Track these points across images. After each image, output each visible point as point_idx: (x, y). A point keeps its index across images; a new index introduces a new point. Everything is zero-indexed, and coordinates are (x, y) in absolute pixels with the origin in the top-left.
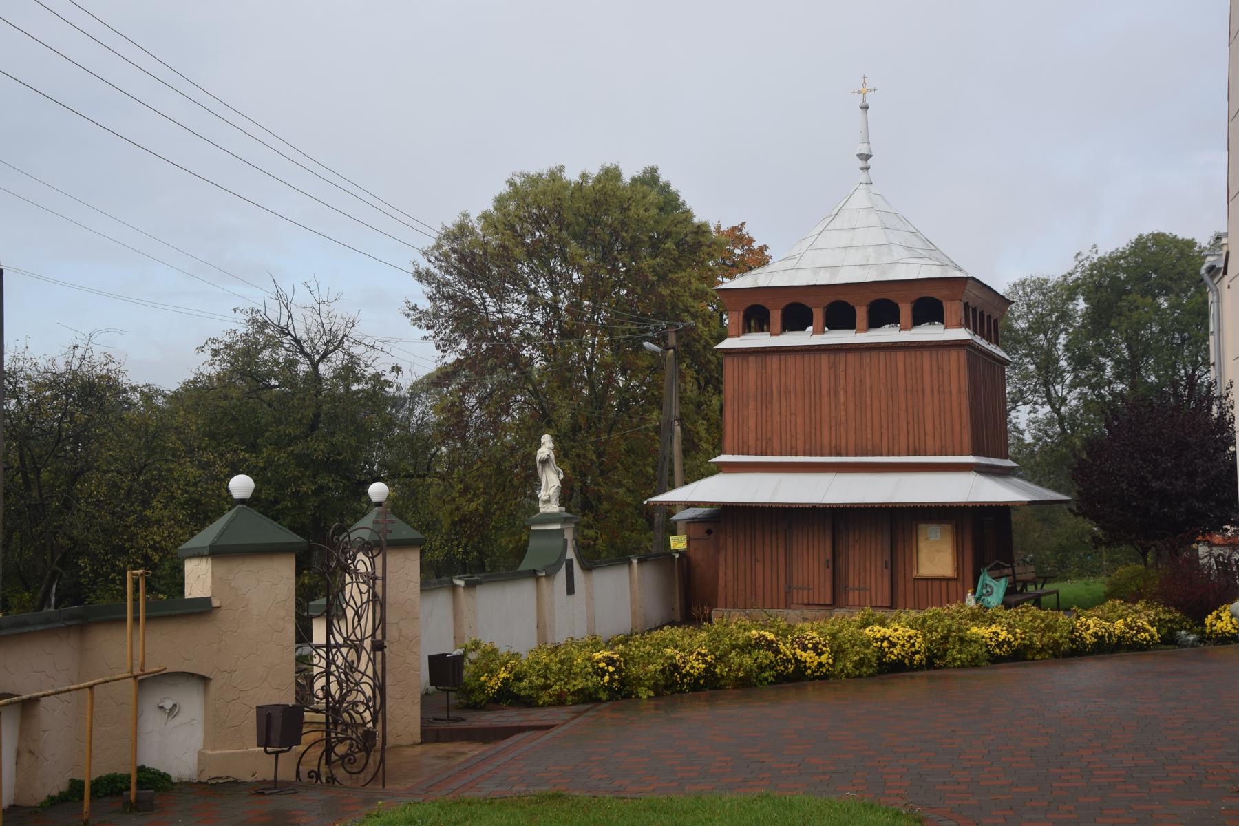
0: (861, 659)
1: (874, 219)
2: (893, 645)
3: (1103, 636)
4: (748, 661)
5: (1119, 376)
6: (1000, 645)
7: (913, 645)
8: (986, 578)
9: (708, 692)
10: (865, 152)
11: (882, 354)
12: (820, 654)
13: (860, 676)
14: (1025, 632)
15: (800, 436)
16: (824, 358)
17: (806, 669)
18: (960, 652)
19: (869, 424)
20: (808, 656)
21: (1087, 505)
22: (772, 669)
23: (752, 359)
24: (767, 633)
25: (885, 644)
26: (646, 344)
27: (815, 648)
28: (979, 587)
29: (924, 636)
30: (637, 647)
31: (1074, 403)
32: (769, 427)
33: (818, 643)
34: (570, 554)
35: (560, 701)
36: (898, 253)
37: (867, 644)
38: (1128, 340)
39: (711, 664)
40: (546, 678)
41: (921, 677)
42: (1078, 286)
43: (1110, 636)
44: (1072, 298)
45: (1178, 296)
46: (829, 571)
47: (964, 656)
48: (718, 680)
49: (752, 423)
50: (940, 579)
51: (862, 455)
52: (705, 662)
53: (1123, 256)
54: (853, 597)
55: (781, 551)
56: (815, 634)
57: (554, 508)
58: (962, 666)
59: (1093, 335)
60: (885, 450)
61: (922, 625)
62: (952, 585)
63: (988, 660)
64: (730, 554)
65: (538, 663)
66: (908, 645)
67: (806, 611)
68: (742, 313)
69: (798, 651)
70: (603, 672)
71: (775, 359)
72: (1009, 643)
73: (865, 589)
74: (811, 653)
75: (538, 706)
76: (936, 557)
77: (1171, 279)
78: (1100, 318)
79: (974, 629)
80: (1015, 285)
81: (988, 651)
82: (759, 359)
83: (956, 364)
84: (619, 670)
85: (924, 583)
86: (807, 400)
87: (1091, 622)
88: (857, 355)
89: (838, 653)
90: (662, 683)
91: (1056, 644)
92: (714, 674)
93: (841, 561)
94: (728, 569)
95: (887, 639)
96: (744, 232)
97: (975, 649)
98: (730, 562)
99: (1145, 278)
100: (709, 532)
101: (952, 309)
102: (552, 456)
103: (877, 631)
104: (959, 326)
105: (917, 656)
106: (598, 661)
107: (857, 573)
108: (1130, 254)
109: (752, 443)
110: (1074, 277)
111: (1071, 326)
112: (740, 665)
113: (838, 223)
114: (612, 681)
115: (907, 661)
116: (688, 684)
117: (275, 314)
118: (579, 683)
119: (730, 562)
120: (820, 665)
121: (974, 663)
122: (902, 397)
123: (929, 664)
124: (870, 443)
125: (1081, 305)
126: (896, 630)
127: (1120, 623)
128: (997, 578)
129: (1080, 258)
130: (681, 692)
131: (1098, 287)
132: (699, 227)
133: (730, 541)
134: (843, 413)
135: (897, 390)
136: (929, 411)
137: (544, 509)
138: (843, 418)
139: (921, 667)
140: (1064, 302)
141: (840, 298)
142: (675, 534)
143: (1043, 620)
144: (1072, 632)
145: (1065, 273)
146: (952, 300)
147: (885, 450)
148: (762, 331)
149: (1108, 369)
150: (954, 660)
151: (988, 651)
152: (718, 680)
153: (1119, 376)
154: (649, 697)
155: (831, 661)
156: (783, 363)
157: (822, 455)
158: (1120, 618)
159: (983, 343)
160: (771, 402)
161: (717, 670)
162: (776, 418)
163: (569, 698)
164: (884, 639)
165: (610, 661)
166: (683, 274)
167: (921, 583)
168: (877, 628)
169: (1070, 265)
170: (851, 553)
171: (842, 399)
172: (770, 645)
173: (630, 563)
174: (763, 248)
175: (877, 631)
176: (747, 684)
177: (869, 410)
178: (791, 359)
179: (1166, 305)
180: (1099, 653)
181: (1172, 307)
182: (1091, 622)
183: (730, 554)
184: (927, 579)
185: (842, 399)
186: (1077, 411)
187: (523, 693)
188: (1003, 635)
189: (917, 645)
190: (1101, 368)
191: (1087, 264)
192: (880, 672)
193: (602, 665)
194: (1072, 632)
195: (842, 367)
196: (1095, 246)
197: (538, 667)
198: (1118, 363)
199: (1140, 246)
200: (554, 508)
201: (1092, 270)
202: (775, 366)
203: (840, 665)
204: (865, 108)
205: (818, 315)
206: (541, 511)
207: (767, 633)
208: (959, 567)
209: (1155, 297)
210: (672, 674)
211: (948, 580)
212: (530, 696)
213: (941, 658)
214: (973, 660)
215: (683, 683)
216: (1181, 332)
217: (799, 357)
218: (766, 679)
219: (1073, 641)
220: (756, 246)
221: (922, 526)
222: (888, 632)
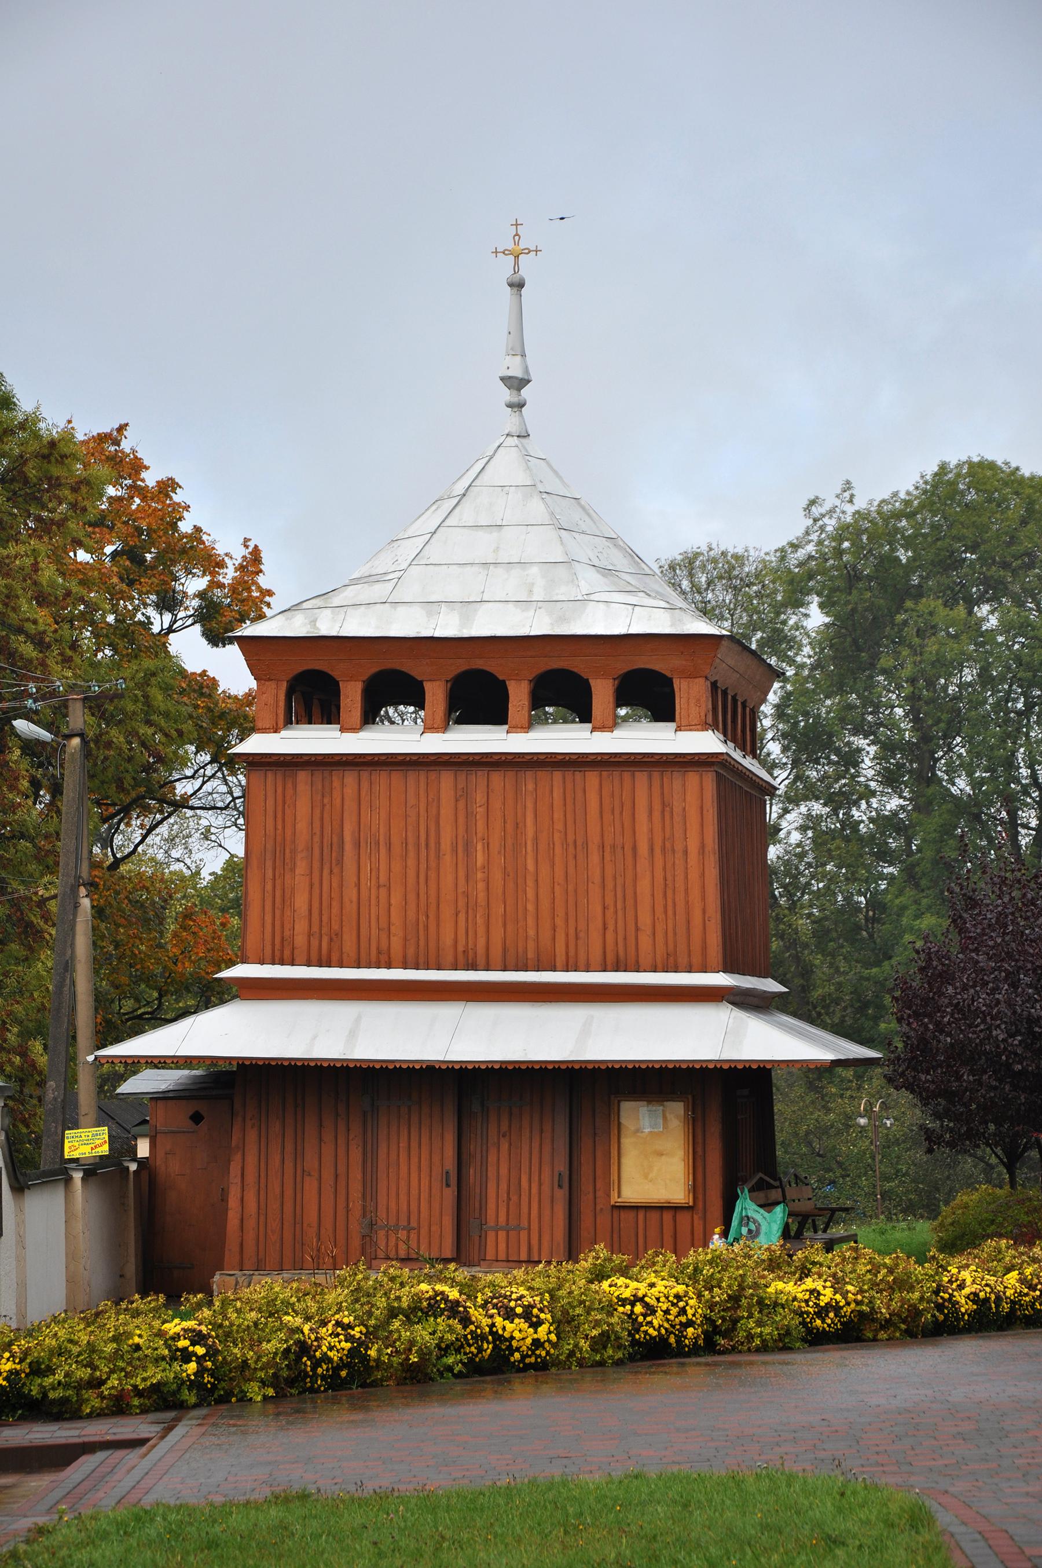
0: (602, 1334)
1: (537, 509)
2: (651, 1310)
3: (987, 1300)
4: (423, 1334)
5: (890, 779)
6: (821, 1312)
7: (683, 1311)
8: (746, 1206)
9: (356, 1391)
10: (517, 372)
11: (558, 775)
12: (536, 1325)
13: (601, 1364)
14: (861, 1291)
15: (397, 930)
16: (446, 779)
17: (512, 1350)
18: (760, 1323)
19: (530, 907)
20: (516, 1329)
21: (915, 1068)
22: (458, 1351)
23: (303, 776)
24: (446, 1289)
25: (639, 1309)
26: (21, 725)
27: (527, 1315)
28: (735, 1223)
29: (699, 1296)
30: (239, 1311)
31: (795, 837)
32: (335, 910)
33: (531, 1306)
35: (118, 1406)
36: (589, 580)
37: (610, 1309)
38: (913, 700)
39: (361, 1343)
40: (95, 1368)
41: (698, 1364)
42: (811, 576)
43: (998, 1299)
44: (796, 602)
45: (1020, 604)
46: (450, 1194)
47: (767, 1330)
48: (369, 1370)
49: (301, 901)
50: (661, 1208)
51: (517, 969)
52: (349, 1338)
53: (907, 511)
54: (496, 1243)
55: (356, 1154)
56: (522, 1291)
58: (764, 1348)
59: (838, 687)
60: (560, 960)
61: (694, 1277)
62: (683, 1218)
63: (804, 1340)
64: (251, 1159)
65: (75, 1343)
66: (674, 1311)
68: (284, 685)
69: (499, 1320)
70: (186, 1356)
71: (350, 778)
72: (837, 1309)
73: (518, 1229)
74: (521, 1323)
75: (81, 1418)
76: (653, 1161)
77: (1005, 565)
78: (853, 650)
79: (780, 1285)
80: (672, 567)
81: (804, 1323)
82: (318, 775)
83: (697, 794)
84: (212, 1353)
85: (632, 1214)
86: (411, 862)
87: (966, 1275)
88: (511, 774)
89: (565, 1323)
90: (285, 1373)
91: (915, 1312)
92: (366, 1358)
93: (472, 1173)
94: (252, 1184)
95: (641, 1300)
96: (126, 445)
97: (785, 1318)
98: (251, 1178)
99: (950, 562)
100: (197, 1118)
101: (690, 694)
103: (624, 1287)
104: (704, 726)
105: (690, 1330)
106: (176, 1337)
107: (503, 1196)
108: (922, 506)
109: (300, 940)
110: (801, 554)
111: (791, 662)
112: (412, 1343)
113: (466, 514)
114: (199, 1373)
115: (672, 1340)
116: (323, 1377)
118: (155, 1375)
119: (251, 1178)
120: (537, 1343)
121: (782, 1344)
122: (595, 858)
123: (708, 1345)
124: (531, 945)
125: (815, 618)
126: (652, 1285)
127: (1013, 1277)
128: (768, 1206)
129: (816, 511)
130: (313, 1390)
131: (853, 577)
132: (53, 444)
133: (252, 1136)
134: (481, 886)
135: (586, 843)
136: (644, 886)
138: (482, 896)
139: (695, 1350)
140: (778, 609)
141: (479, 664)
142: (76, 1126)
143: (891, 1271)
144: (936, 1293)
145: (783, 542)
146: (692, 676)
147: (560, 960)
148: (329, 723)
149: (868, 762)
150: (750, 1337)
151: (804, 1323)
152: (369, 1370)
153: (890, 779)
154: (266, 1398)
155: (553, 1337)
156: (365, 785)
157: (439, 968)
158: (1008, 1270)
159: (737, 755)
160: (340, 862)
161: (373, 1353)
162: (350, 893)
163: (136, 1402)
164: (636, 1299)
165: (198, 1338)
166: (22, 549)
167: (623, 1214)
168: (621, 1281)
169: (796, 526)
170: (492, 1158)
171: (480, 859)
172: (454, 1309)
173: (68, 1180)
174: (168, 486)
175: (624, 1287)
176: (418, 1377)
177: (530, 883)
178: (381, 778)
179: (993, 622)
180: (979, 1330)
181: (1006, 627)
182: (966, 1275)
183: (251, 1159)
184: (636, 1208)
185: (480, 859)
186: (801, 856)
187: (52, 1395)
188: (828, 1295)
189: (690, 1312)
190: (851, 759)
191: (831, 524)
192: (632, 1358)
193: (183, 1343)
194: (936, 1293)
195: (480, 798)
196: (848, 486)
197: (75, 1349)
198: (887, 748)
199: (941, 489)
201: (839, 538)
202: (350, 790)
203: (567, 1347)
204: (518, 285)
205: (436, 693)
207: (446, 1289)
208: (696, 1187)
209: (971, 603)
210: (298, 1359)
211: (675, 1209)
212: (64, 1401)
213: (727, 1334)
214: (781, 1337)
215: (315, 1374)
216: (1027, 687)
217: (397, 777)
218: (450, 1369)
219: (940, 1307)
220: (150, 479)
221: (627, 1108)
222: (642, 1289)
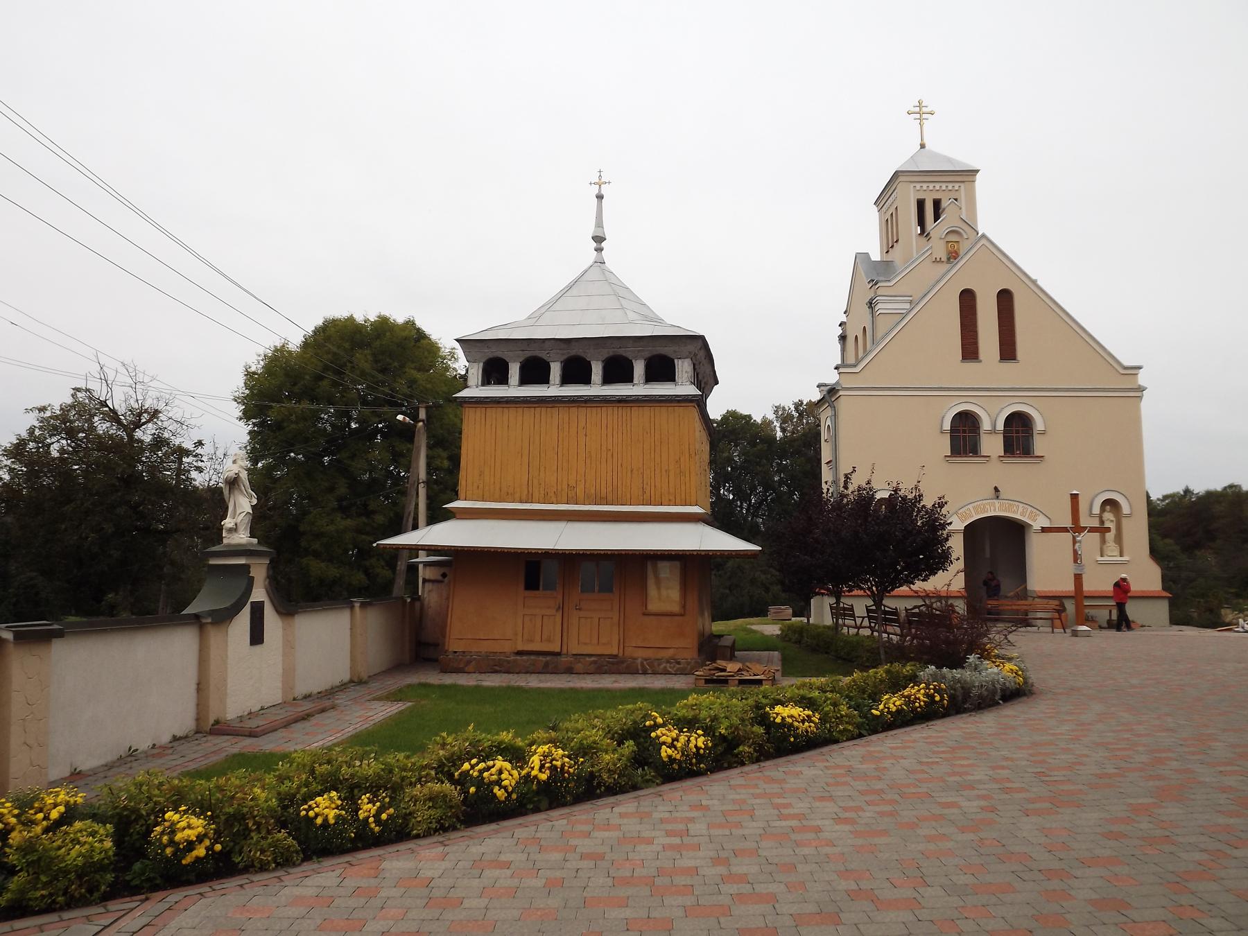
34: (259, 594)
57: (243, 538)
67: (523, 684)
102: (244, 475)
117: (100, 392)
137: (230, 540)
173: (352, 608)
200: (243, 538)
206: (225, 541)
